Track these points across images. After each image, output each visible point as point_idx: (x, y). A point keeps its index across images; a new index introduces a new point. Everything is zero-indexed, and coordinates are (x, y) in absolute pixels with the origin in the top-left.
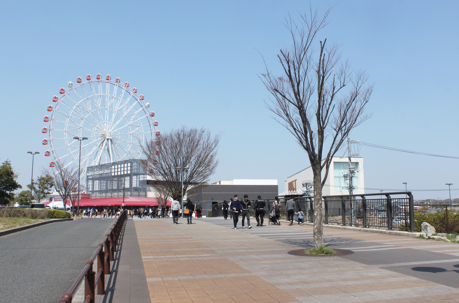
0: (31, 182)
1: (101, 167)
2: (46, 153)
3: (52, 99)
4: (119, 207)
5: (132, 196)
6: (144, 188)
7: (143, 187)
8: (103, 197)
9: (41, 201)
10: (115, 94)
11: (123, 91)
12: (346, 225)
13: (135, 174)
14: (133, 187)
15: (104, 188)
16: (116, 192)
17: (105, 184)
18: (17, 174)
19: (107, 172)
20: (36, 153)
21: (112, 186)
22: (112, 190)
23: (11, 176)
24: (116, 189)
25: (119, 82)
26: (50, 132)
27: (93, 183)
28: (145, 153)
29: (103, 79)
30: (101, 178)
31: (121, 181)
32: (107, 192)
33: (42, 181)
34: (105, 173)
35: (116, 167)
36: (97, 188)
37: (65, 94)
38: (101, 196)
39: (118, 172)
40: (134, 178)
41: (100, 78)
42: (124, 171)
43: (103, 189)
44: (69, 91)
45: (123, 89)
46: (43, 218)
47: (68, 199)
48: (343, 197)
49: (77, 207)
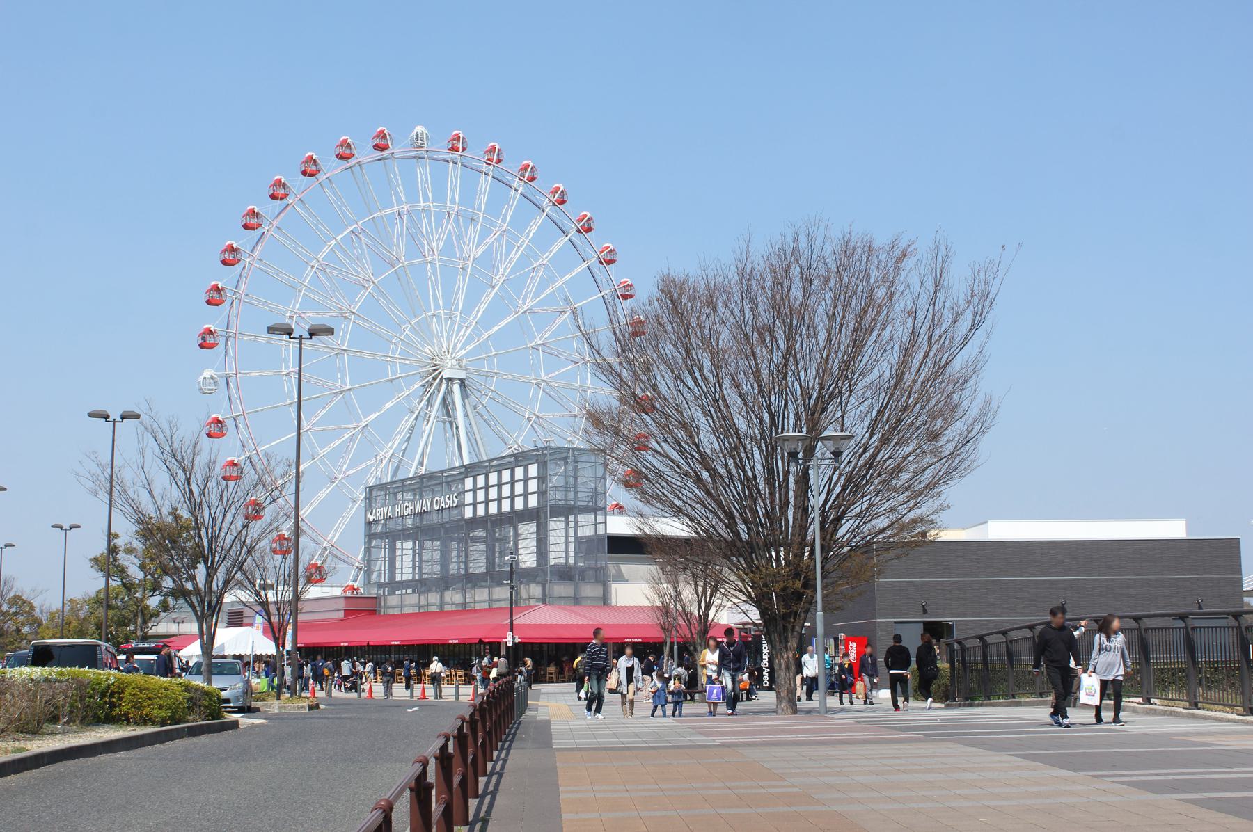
1: (425, 483)
3: (240, 222)
4: (494, 648)
5: (548, 600)
6: (596, 569)
7: (593, 564)
12: (1199, 705)
13: (558, 511)
14: (552, 562)
15: (432, 570)
16: (483, 584)
17: (437, 555)
19: (443, 505)
21: (466, 563)
22: (467, 578)
27: (392, 550)
28: (606, 370)
30: (422, 530)
31: (503, 540)
32: (447, 588)
34: (436, 508)
35: (481, 481)
36: (406, 573)
37: (289, 200)
38: (423, 602)
40: (556, 524)
42: (512, 497)
45: (511, 187)
48: (1241, 616)
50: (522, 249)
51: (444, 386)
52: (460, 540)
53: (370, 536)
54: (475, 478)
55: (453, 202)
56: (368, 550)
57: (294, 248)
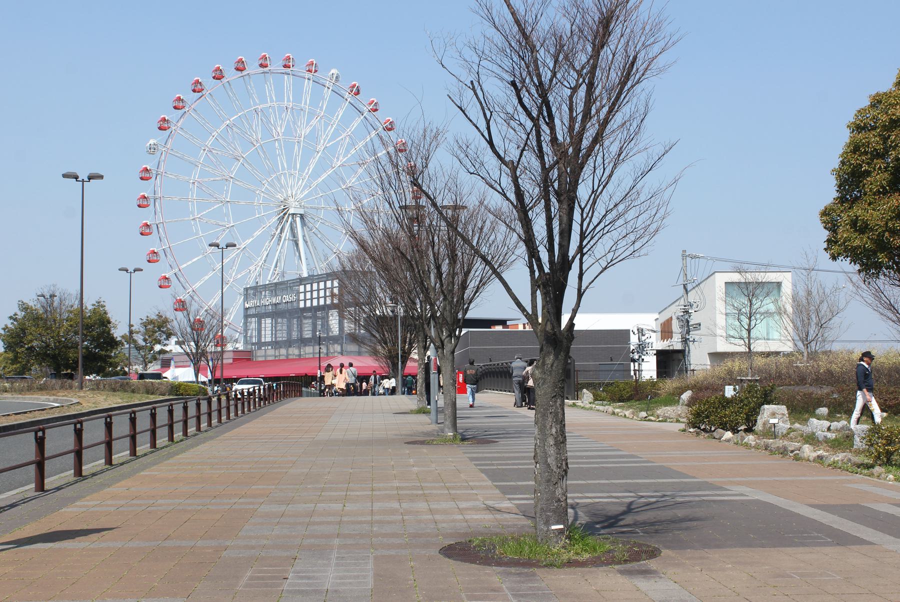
0: (128, 330)
1: (276, 288)
2: (141, 227)
8: (281, 358)
9: (148, 367)
10: (306, 100)
11: (327, 93)
15: (282, 336)
16: (310, 344)
17: (285, 328)
18: (116, 323)
19: (288, 300)
20: (135, 271)
22: (301, 341)
23: (106, 326)
25: (316, 71)
26: (157, 203)
27: (260, 324)
29: (276, 65)
30: (276, 313)
32: (290, 346)
33: (149, 327)
36: (267, 337)
38: (277, 354)
39: (312, 299)
41: (268, 62)
43: (281, 339)
44: (195, 102)
46: (164, 395)
47: (202, 363)
49: (220, 379)
50: (334, 126)
51: (290, 218)
52: (298, 317)
53: (246, 316)
54: (305, 285)
55: (289, 100)
56: (245, 323)
57: (192, 139)
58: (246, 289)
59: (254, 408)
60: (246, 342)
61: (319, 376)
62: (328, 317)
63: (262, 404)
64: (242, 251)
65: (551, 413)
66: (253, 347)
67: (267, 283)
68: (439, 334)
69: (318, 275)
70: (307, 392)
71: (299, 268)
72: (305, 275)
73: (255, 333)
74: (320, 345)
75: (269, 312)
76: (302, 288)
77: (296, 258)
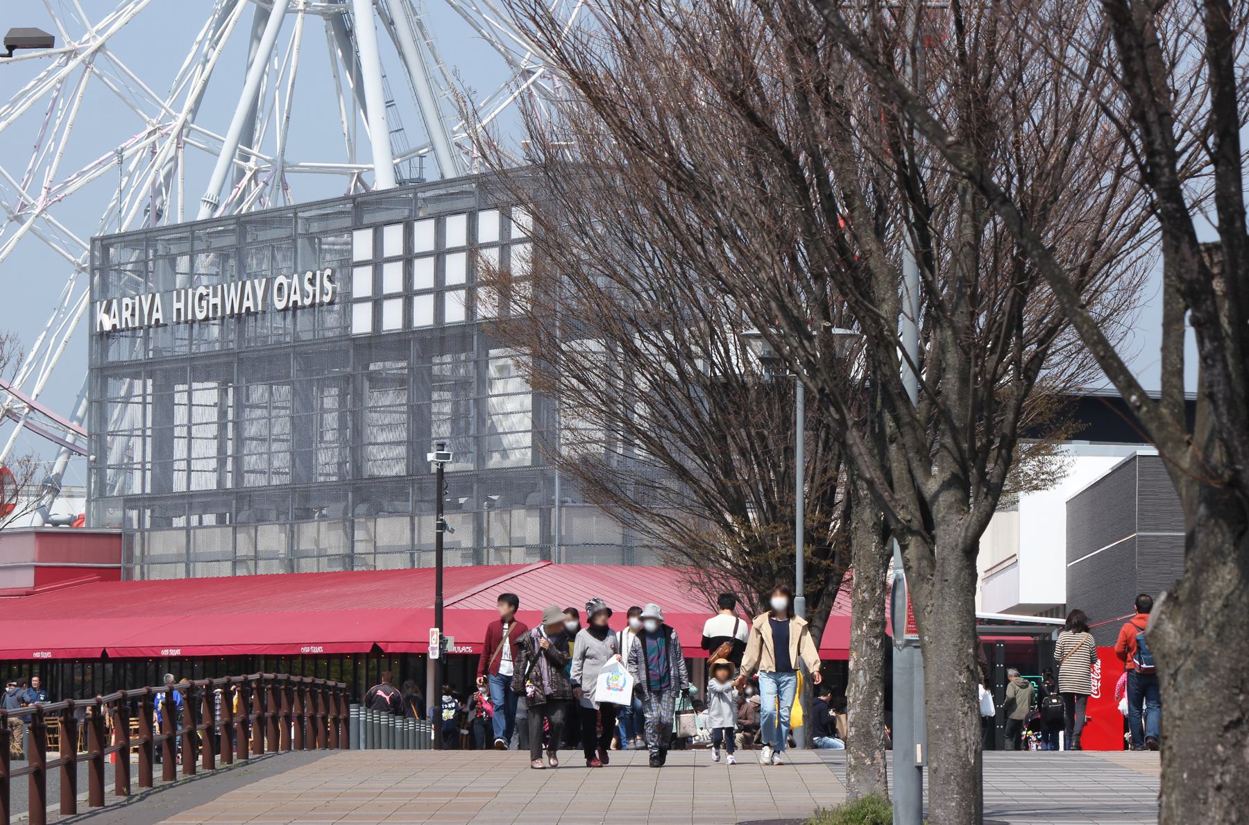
16: (399, 505)
17: (282, 427)
22: (357, 490)
24: (398, 478)
27: (164, 407)
32: (306, 515)
34: (280, 305)
38: (244, 549)
39: (408, 295)
54: (378, 229)
56: (99, 405)
58: (103, 244)
59: (119, 792)
60: (99, 494)
61: (434, 655)
62: (484, 382)
63: (158, 772)
64: (87, 64)
65: (1219, 788)
66: (134, 514)
67: (203, 213)
68: (910, 471)
69: (444, 182)
70: (372, 729)
71: (356, 143)
72: (383, 181)
73: (140, 451)
74: (440, 510)
75: (209, 356)
76: (362, 243)
77: (345, 103)
